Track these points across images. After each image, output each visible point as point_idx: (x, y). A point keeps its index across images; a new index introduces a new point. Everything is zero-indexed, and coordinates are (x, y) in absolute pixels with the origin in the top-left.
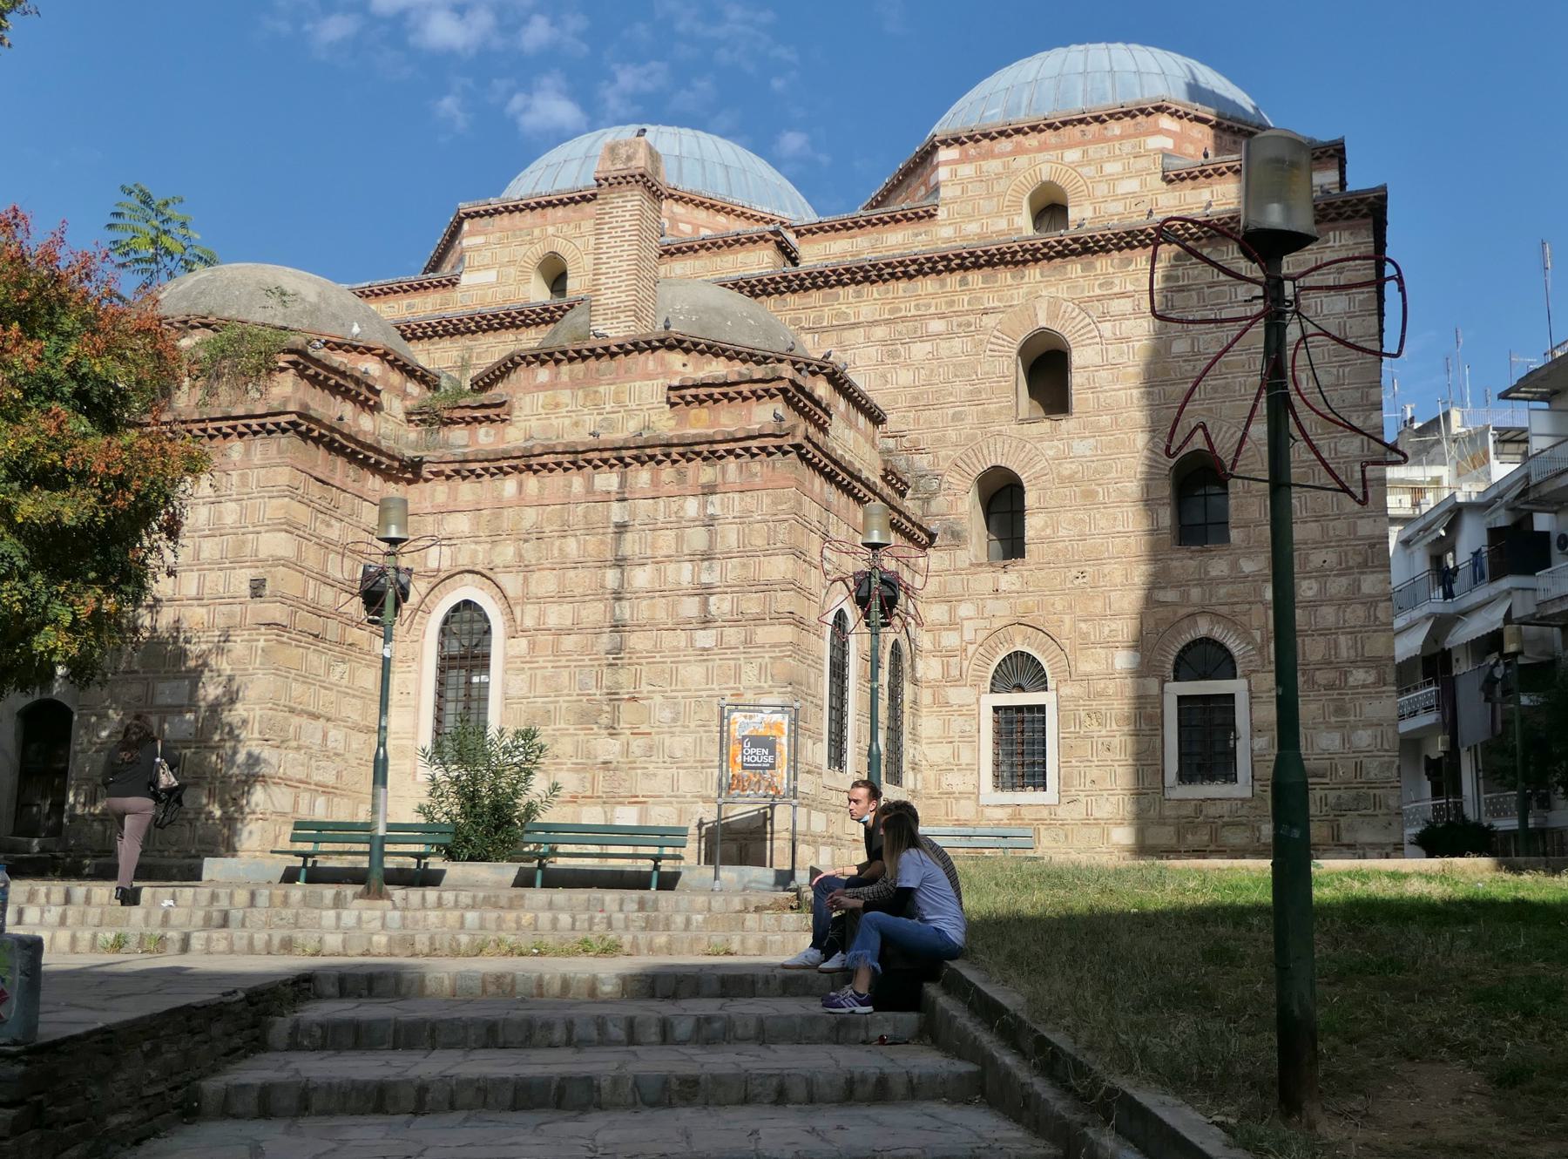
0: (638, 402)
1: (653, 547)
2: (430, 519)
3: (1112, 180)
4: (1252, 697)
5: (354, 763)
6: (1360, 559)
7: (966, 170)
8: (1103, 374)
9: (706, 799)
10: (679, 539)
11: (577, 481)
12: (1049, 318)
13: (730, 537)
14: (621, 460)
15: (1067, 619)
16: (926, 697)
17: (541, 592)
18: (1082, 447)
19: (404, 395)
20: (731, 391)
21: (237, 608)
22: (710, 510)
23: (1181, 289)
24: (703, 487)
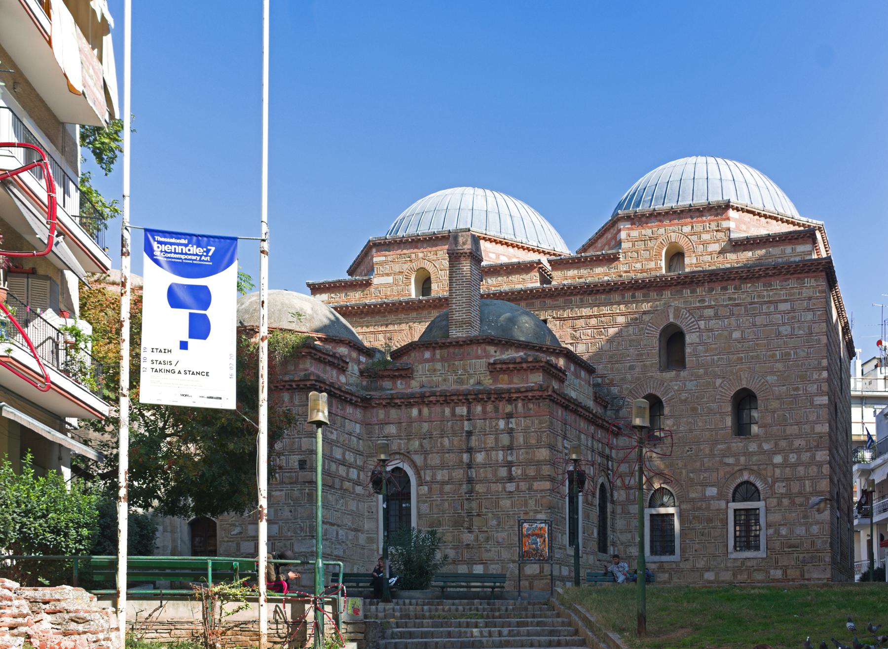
0: (475, 371)
1: (485, 443)
2: (377, 427)
3: (705, 244)
4: (767, 509)
5: (350, 545)
6: (815, 444)
7: (635, 233)
8: (700, 347)
9: (514, 562)
10: (497, 439)
11: (447, 411)
12: (674, 318)
13: (520, 439)
14: (468, 400)
15: (684, 471)
16: (619, 509)
17: (433, 464)
18: (690, 385)
19: (359, 362)
20: (518, 366)
21: (294, 474)
22: (510, 426)
23: (737, 305)
24: (507, 414)
